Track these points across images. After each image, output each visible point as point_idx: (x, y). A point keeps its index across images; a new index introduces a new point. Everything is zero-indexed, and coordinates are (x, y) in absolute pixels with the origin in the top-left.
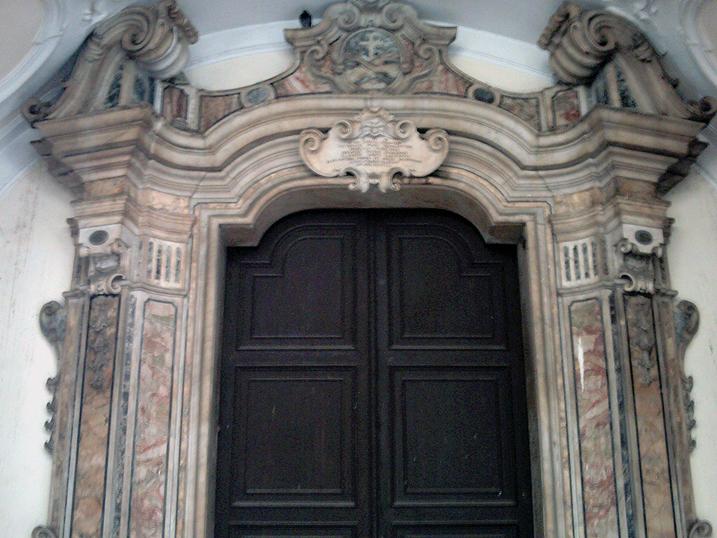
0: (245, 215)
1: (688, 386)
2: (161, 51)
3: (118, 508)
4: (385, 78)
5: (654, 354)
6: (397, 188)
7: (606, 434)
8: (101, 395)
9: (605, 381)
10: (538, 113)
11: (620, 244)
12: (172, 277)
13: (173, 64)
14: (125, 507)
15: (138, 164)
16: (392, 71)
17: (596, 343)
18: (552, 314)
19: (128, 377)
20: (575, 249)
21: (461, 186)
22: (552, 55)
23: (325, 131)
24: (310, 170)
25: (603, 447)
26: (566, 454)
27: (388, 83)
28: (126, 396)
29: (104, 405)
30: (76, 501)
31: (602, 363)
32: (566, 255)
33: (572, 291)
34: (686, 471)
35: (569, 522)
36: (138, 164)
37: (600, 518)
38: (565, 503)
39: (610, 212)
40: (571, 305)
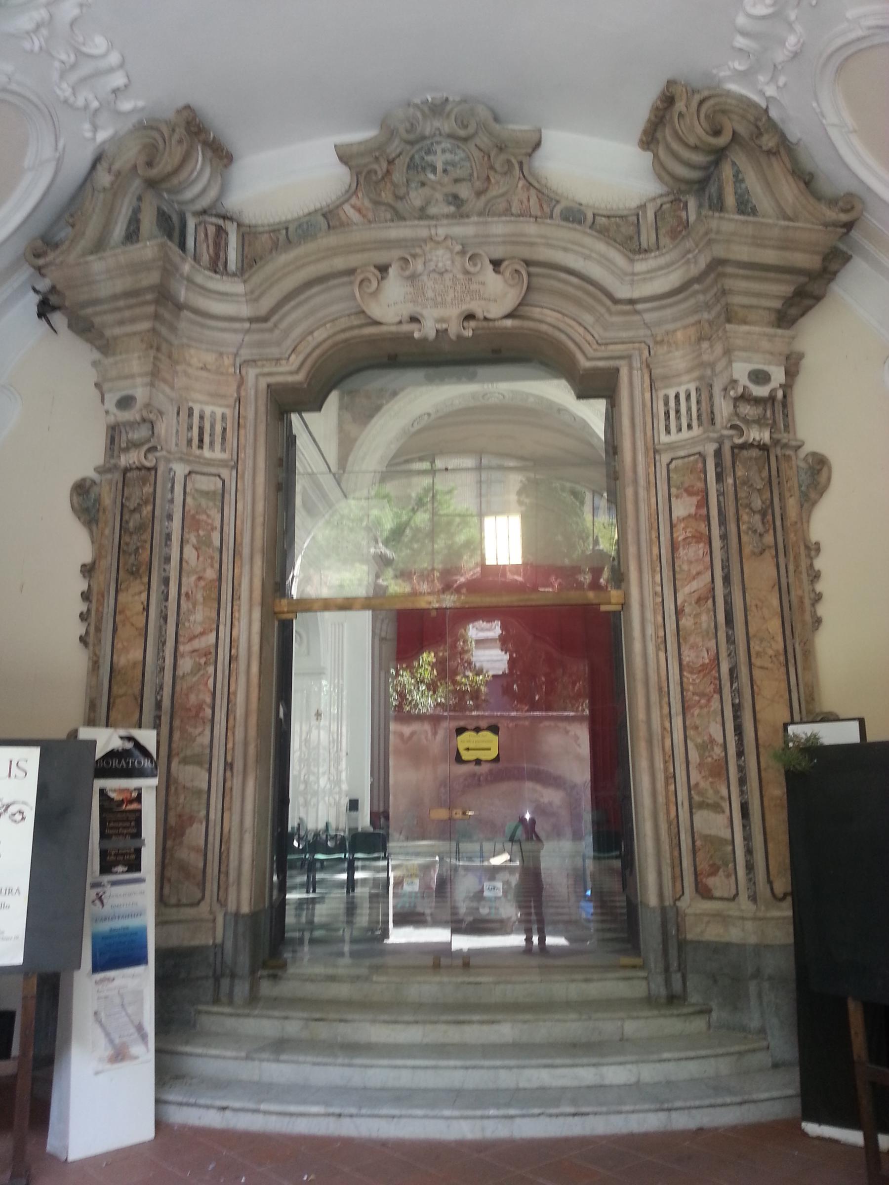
0: (297, 371)
1: (813, 553)
2: (183, 175)
3: (158, 705)
4: (455, 200)
5: (769, 517)
6: (469, 333)
7: (708, 611)
8: (138, 581)
9: (707, 549)
10: (639, 233)
11: (729, 388)
12: (218, 446)
13: (204, 191)
14: (166, 703)
15: (167, 316)
16: (464, 191)
17: (698, 507)
18: (583, 246)
19: (168, 560)
20: (677, 397)
21: (544, 328)
22: (656, 156)
23: (383, 269)
24: (370, 317)
25: (704, 626)
26: (661, 634)
27: (458, 207)
28: (166, 581)
29: (141, 593)
30: (111, 700)
31: (703, 527)
32: (666, 403)
33: (671, 447)
34: (809, 653)
35: (666, 710)
36: (167, 316)
37: (701, 708)
38: (660, 689)
39: (719, 349)
40: (671, 462)
